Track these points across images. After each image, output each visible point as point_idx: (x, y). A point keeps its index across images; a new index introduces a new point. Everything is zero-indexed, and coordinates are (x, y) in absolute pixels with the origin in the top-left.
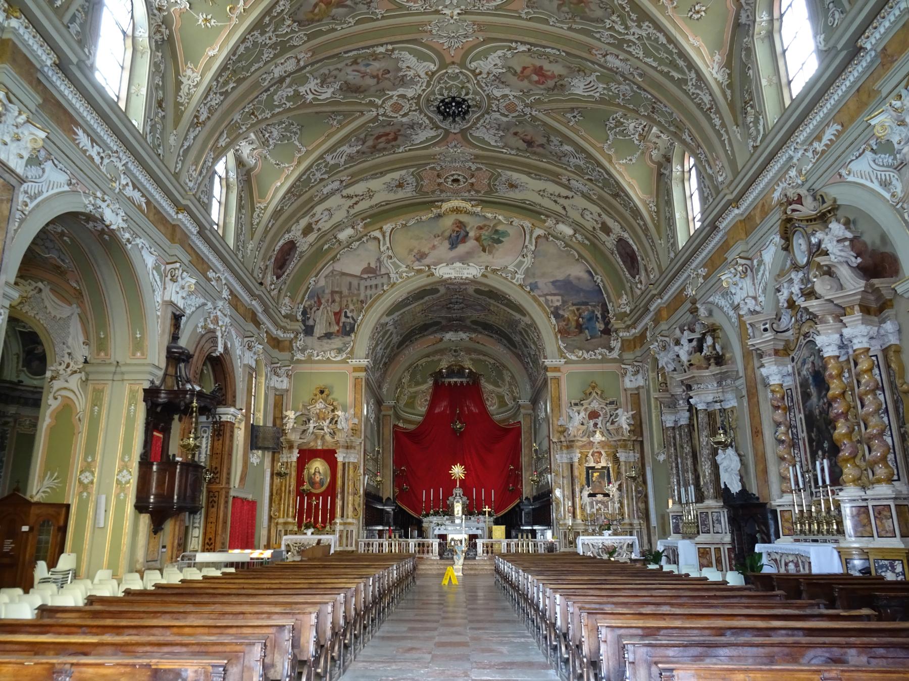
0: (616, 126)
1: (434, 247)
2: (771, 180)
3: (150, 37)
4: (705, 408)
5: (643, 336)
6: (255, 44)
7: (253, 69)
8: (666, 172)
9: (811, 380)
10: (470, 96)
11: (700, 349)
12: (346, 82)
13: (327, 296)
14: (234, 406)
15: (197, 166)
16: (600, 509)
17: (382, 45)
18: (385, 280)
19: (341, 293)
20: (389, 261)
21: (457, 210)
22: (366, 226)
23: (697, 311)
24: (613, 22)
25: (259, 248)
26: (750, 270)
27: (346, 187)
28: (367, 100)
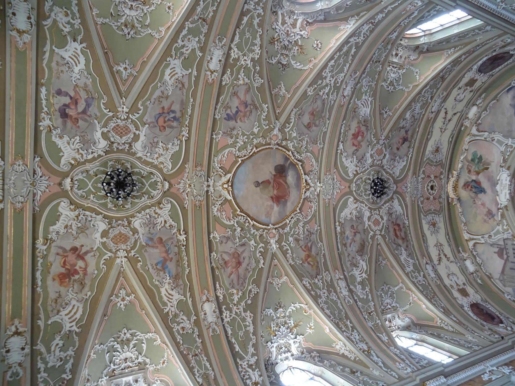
0: (393, 85)
1: (483, 204)
3: (315, 365)
6: (326, 303)
7: (341, 307)
10: (371, 177)
12: (357, 252)
17: (336, 228)
18: (509, 243)
20: (493, 237)
21: (455, 188)
22: (465, 251)
24: (323, 94)
25: (473, 332)
28: (370, 240)
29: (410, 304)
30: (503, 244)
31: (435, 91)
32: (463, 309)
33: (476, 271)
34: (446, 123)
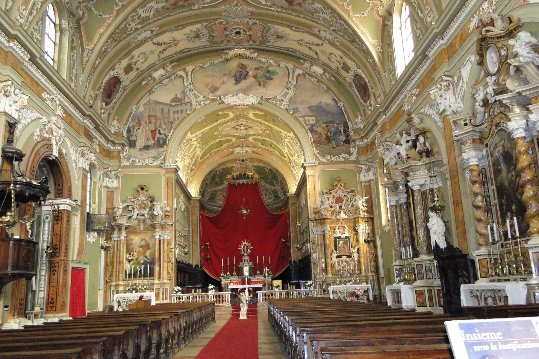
1: (223, 83)
2: (468, 14)
4: (419, 188)
5: (373, 143)
8: (389, 23)
9: (501, 159)
11: (415, 146)
13: (146, 119)
14: (70, 198)
15: (26, 6)
16: (345, 266)
18: (188, 106)
19: (155, 116)
20: (191, 93)
21: (240, 56)
22: (173, 67)
23: (412, 121)
26: (452, 85)
27: (157, 35)
29: (101, 15)
30: (186, 102)
31: (342, 34)
32: (110, 70)
33: (155, 80)
34: (308, 45)
